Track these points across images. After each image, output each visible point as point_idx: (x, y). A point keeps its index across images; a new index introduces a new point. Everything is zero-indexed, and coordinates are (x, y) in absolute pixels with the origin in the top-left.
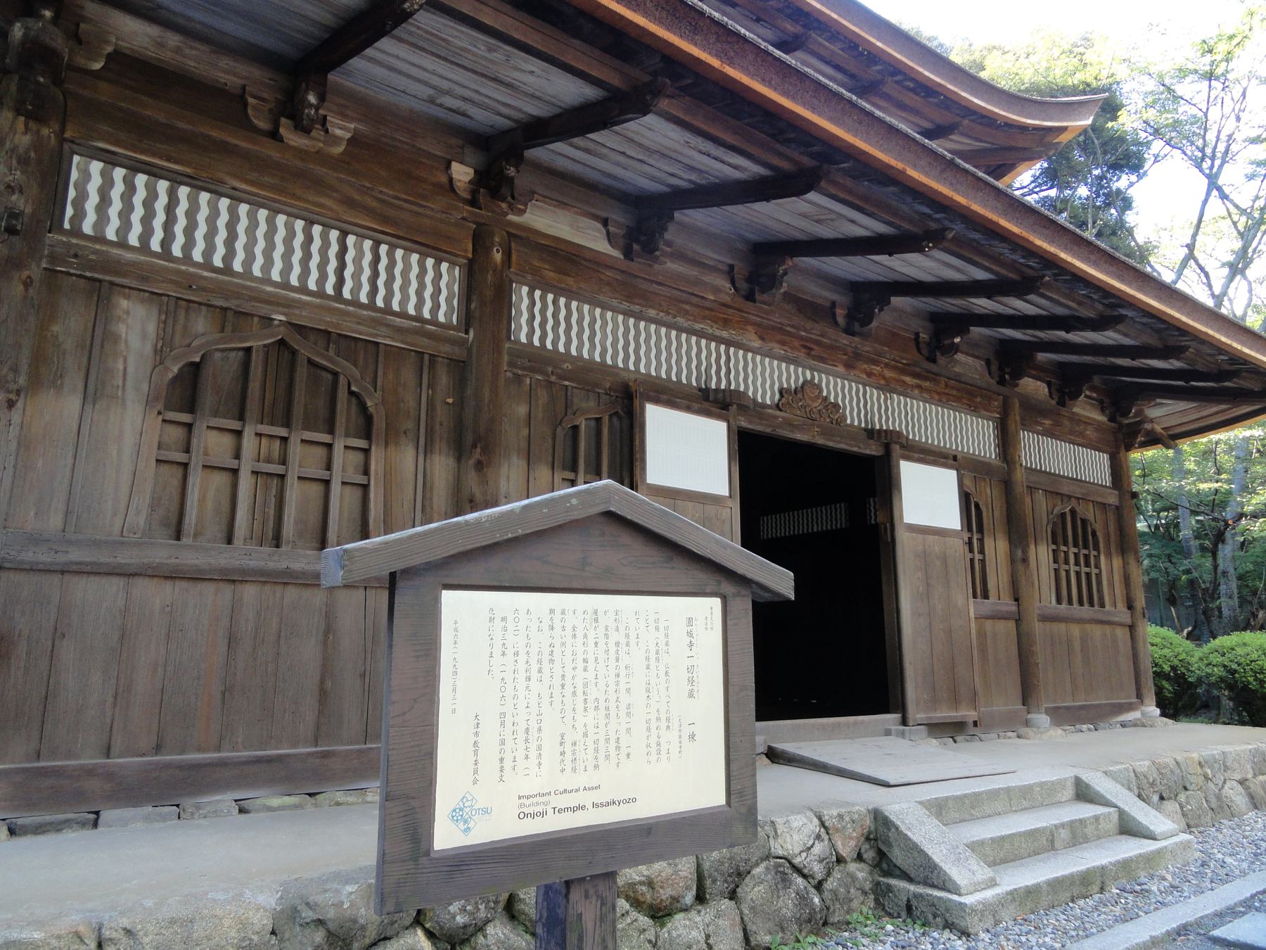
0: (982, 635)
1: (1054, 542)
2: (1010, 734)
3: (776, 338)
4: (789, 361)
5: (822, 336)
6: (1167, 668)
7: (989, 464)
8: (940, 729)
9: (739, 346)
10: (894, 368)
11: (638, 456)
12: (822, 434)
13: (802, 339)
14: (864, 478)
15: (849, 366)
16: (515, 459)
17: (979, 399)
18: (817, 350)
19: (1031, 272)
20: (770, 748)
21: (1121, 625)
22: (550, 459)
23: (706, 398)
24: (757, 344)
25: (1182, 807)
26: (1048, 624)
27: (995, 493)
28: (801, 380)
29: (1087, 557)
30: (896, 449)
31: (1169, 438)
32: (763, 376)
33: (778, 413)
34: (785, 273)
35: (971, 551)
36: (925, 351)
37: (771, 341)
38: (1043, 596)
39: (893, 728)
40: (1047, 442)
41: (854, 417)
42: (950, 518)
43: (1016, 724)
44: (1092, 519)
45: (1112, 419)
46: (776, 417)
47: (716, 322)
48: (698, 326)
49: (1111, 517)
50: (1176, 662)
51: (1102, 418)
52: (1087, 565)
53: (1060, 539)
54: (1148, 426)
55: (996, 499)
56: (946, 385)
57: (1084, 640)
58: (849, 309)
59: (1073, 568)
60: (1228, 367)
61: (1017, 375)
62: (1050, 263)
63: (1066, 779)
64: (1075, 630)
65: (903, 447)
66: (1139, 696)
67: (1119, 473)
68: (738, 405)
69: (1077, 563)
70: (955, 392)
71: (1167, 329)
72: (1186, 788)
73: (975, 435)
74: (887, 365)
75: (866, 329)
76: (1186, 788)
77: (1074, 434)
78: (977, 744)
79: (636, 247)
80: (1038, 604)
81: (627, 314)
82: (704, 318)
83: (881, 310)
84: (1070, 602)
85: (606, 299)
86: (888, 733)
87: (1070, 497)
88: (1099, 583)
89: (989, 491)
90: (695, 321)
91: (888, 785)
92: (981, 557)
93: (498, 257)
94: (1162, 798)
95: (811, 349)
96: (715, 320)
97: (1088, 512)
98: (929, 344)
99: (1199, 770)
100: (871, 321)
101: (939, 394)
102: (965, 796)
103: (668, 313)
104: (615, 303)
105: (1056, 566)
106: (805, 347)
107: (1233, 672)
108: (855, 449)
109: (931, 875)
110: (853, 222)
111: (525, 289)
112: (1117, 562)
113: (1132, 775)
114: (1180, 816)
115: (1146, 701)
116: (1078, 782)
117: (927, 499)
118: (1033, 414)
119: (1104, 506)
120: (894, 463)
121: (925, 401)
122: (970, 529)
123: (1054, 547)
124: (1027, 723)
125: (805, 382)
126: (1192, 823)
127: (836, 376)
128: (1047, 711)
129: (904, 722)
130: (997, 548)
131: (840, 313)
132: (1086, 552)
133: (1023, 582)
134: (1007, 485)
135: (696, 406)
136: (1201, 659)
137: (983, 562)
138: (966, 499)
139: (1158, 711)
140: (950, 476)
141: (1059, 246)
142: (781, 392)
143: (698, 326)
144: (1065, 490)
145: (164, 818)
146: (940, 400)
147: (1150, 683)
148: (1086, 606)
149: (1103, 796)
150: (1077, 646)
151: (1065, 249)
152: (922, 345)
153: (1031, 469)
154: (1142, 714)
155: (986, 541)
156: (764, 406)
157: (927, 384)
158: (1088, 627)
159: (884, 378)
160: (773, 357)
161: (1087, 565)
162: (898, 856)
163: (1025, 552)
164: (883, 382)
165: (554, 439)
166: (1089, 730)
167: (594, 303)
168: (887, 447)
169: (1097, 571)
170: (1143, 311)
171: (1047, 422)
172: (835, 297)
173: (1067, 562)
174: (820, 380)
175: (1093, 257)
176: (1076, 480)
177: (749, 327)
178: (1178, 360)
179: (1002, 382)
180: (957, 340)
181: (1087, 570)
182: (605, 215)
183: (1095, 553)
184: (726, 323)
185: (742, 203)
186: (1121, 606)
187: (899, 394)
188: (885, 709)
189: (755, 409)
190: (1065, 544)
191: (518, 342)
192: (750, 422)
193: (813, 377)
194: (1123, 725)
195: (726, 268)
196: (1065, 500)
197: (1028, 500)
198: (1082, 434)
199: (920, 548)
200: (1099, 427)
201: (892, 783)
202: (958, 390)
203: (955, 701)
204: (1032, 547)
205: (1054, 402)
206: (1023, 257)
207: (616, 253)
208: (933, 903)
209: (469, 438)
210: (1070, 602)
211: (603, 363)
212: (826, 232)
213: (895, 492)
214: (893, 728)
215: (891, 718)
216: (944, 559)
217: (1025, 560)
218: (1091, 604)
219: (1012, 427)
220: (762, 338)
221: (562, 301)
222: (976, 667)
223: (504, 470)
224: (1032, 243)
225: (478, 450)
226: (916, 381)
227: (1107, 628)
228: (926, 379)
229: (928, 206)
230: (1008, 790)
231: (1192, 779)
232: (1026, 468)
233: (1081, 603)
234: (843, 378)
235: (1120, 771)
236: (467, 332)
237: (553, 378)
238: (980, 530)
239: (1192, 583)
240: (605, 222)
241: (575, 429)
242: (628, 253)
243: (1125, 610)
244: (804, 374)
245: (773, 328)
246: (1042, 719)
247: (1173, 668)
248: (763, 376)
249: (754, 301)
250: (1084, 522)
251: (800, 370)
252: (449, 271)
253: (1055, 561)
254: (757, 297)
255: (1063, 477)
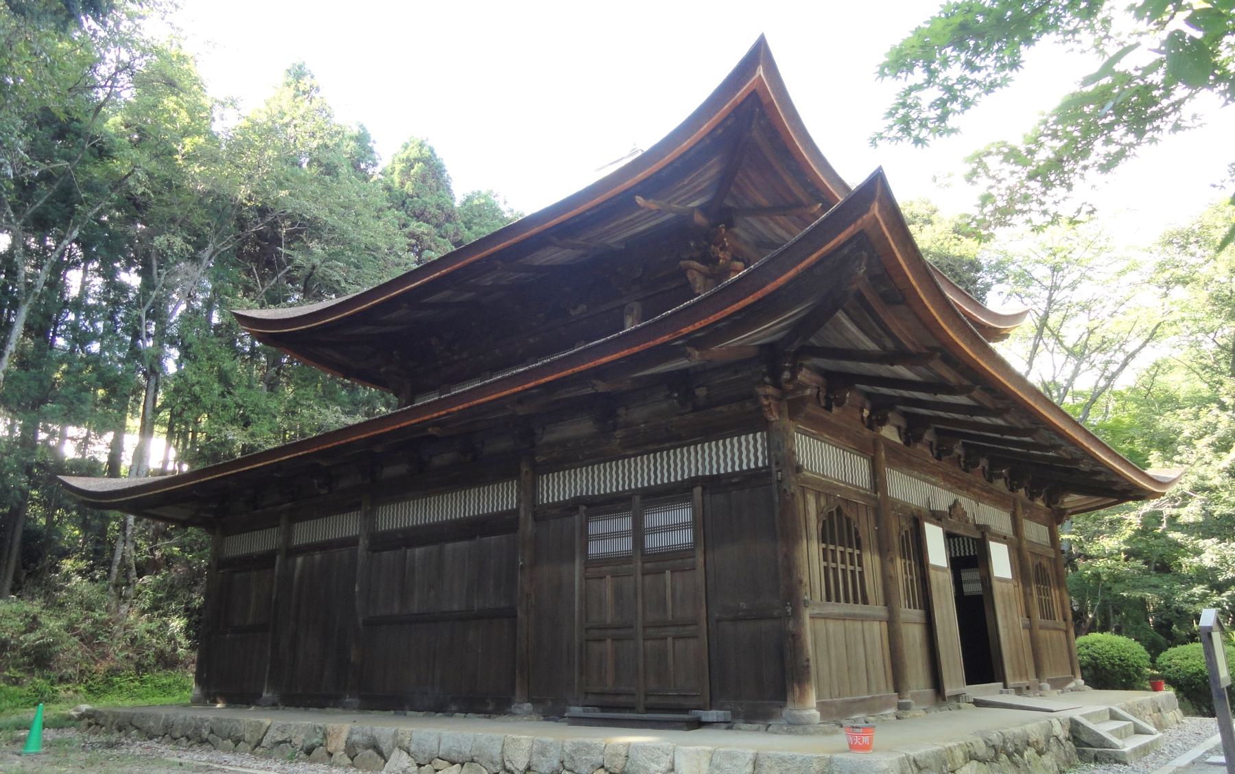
45: (1048, 506)
59: (840, 566)
66: (1073, 673)
69: (843, 562)
97: (1045, 563)
107: (1095, 659)
109: (1102, 742)
119: (1049, 558)
123: (824, 546)
129: (1005, 686)
137: (861, 573)
145: (758, 730)
162: (1085, 738)
168: (983, 533)
173: (834, 561)
188: (991, 679)
207: (898, 440)
208: (1108, 754)
246: (1047, 686)
253: (825, 559)
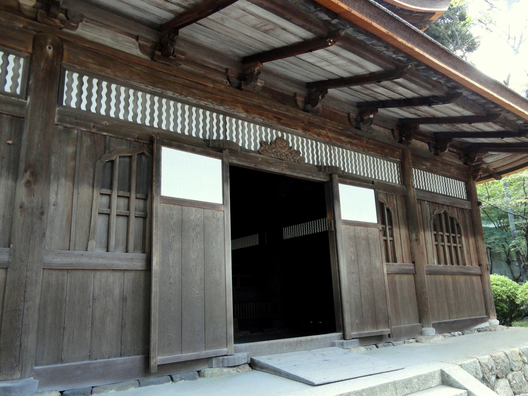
0: (392, 283)
1: (435, 230)
2: (411, 340)
3: (255, 112)
4: (266, 126)
5: (287, 111)
6: (505, 297)
7: (394, 186)
8: (364, 340)
9: (232, 116)
10: (335, 132)
11: (154, 179)
12: (289, 168)
13: (275, 113)
14: (317, 196)
15: (305, 129)
16: (63, 181)
17: (387, 151)
18: (285, 120)
19: (401, 64)
20: (252, 360)
21: (476, 275)
22: (91, 181)
23: (208, 146)
24: (243, 115)
25: (510, 382)
26: (433, 277)
27: (399, 203)
28: (275, 137)
29: (454, 238)
30: (336, 177)
31: (497, 175)
32: (249, 135)
33: (258, 155)
34: (259, 73)
35: (385, 235)
36: (354, 123)
37: (254, 113)
38: (430, 259)
39: (337, 341)
40: (429, 175)
41: (309, 158)
42: (370, 215)
43: (414, 333)
44: (457, 217)
45: (465, 163)
46: (257, 158)
47: (215, 101)
48: (202, 103)
49: (467, 216)
50: (510, 294)
51: (460, 163)
52: (455, 242)
53: (438, 228)
54: (485, 166)
55: (397, 207)
56: (367, 142)
57: (454, 283)
58: (305, 98)
60: (523, 128)
61: (409, 138)
62: (411, 57)
63: (435, 372)
64: (449, 278)
65: (340, 176)
67: (471, 192)
68: (230, 149)
69: (449, 241)
70: (372, 146)
71: (486, 103)
72: (512, 370)
73: (387, 171)
74: (330, 130)
75: (315, 108)
76: (512, 370)
77: (445, 171)
78: (391, 348)
79: (158, 53)
80: (427, 265)
81: (153, 94)
82: (208, 98)
83: (323, 97)
84: (446, 263)
85: (135, 84)
86: (333, 345)
87: (443, 205)
88: (462, 252)
89: (395, 202)
90: (200, 99)
91: (313, 385)
92: (391, 239)
93: (50, 51)
94: (497, 378)
95: (281, 119)
96: (215, 100)
97: (455, 214)
98: (356, 120)
99: (520, 358)
100: (317, 104)
101: (362, 146)
102: (363, 390)
103: (182, 94)
104: (143, 86)
105: (437, 243)
106: (275, 117)
108: (310, 177)
110: (284, 29)
111: (75, 76)
112: (471, 241)
113: (478, 365)
114: (509, 388)
115: (491, 316)
116: (443, 373)
117: (356, 205)
118: (420, 160)
119: (462, 210)
120: (334, 185)
121: (355, 151)
122: (383, 222)
123: (435, 233)
124: (421, 333)
125: (278, 137)
126: (516, 391)
127: (298, 135)
128: (434, 326)
129: (344, 337)
130: (400, 234)
131: (300, 100)
132: (454, 235)
133: (416, 252)
134: (405, 198)
135: (199, 149)
136: (522, 292)
137: (393, 241)
138: (380, 207)
139: (498, 322)
140: (370, 193)
141: (413, 43)
142: (261, 143)
143: (202, 103)
144: (440, 200)
146: (364, 151)
147: (493, 307)
148: (455, 265)
149: (457, 383)
150: (451, 288)
151: (418, 46)
152: (352, 120)
153: (420, 189)
154: (490, 324)
155: (394, 229)
156: (250, 151)
157: (355, 141)
158: (457, 277)
159: (328, 137)
160: (256, 123)
161: (455, 242)
163: (417, 236)
164: (327, 140)
165: (94, 168)
166: (459, 335)
167: (129, 86)
168: (331, 175)
169: (460, 245)
170: (472, 91)
171: (428, 164)
172: (296, 90)
173: (443, 241)
174: (288, 137)
175: (436, 53)
176: (447, 195)
177: (239, 105)
178: (495, 123)
179: (401, 141)
180: (372, 116)
181: (455, 245)
182: (136, 34)
183: (459, 235)
184: (222, 102)
185: (269, 61)
186: (475, 265)
187: (339, 147)
189: (244, 153)
190: (442, 231)
191: (68, 106)
192: (239, 160)
193: (283, 136)
194: (479, 331)
195: (224, 71)
196: (441, 206)
197: (418, 206)
198: (449, 171)
199: (352, 234)
200: (458, 168)
201: (316, 383)
202: (374, 145)
203: (376, 323)
204: (422, 233)
205: (433, 153)
206: (394, 53)
209: (22, 166)
210: (446, 263)
211: (135, 122)
212: (277, 43)
213: (336, 202)
214: (337, 341)
215: (335, 336)
216: (367, 240)
217: (417, 240)
218: (458, 263)
219: (407, 166)
220: (247, 111)
221: (95, 81)
222: (389, 303)
223: (53, 187)
224: (396, 40)
225: (28, 174)
226: (347, 140)
227: (468, 277)
228: (355, 138)
229: (326, 14)
230: (394, 383)
231: (516, 364)
232: (417, 189)
233: (452, 263)
234: (302, 137)
235: (471, 364)
236: (26, 99)
237: (94, 130)
238: (391, 223)
239: (518, 253)
240: (137, 38)
241: (112, 162)
242: (152, 56)
243: (478, 266)
244: (276, 134)
245: (255, 106)
246: (430, 331)
247: (508, 297)
248: (249, 135)
249: (242, 90)
250: (452, 219)
251: (274, 131)
252: (16, 61)
253: (436, 241)
254: (243, 87)
255: (439, 194)
